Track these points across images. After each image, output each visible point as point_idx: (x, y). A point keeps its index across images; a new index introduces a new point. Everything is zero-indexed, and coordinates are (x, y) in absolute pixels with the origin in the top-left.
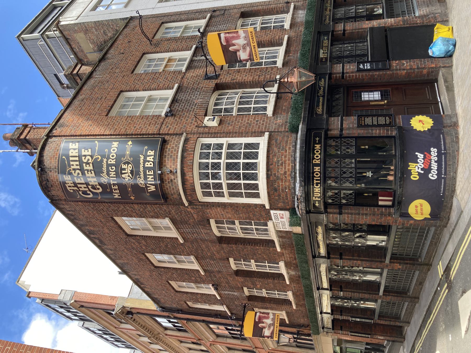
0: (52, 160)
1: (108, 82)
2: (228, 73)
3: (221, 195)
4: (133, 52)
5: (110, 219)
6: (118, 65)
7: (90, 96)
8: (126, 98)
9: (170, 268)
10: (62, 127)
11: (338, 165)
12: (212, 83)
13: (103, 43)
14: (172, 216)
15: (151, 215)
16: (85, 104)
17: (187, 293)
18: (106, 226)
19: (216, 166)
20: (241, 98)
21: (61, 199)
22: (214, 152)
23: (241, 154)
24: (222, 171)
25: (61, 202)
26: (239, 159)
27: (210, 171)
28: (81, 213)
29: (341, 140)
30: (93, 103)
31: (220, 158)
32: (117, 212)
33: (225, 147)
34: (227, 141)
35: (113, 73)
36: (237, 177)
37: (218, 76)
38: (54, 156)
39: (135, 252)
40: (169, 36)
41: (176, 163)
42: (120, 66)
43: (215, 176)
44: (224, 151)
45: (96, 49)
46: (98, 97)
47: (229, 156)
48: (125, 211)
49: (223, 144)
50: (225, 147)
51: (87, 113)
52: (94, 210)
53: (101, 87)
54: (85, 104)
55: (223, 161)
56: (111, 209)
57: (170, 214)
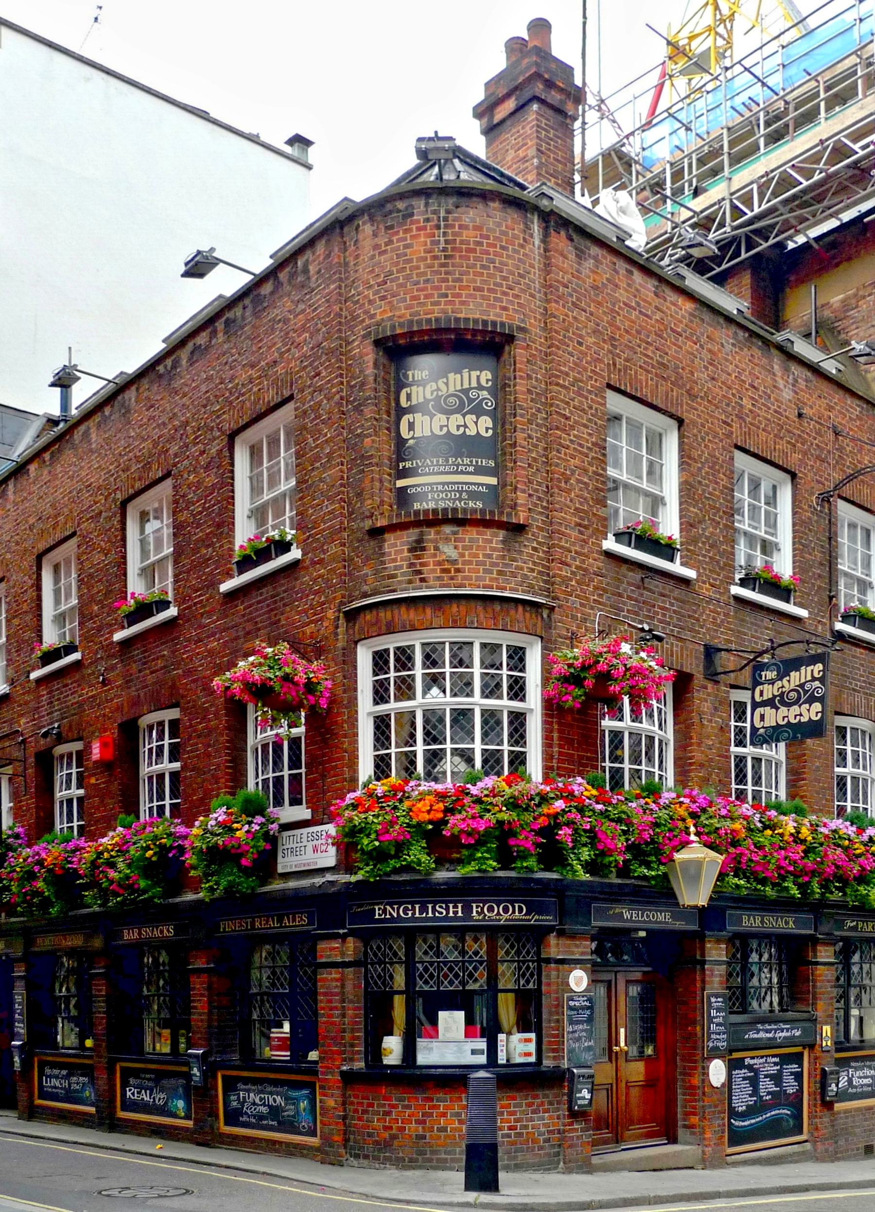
0: (472, 233)
1: (713, 379)
2: (721, 703)
3: (380, 695)
4: (803, 444)
5: (287, 393)
6: (763, 404)
7: (672, 329)
8: (660, 435)
9: (124, 546)
10: (577, 255)
11: (470, 957)
12: (694, 666)
13: (843, 336)
14: (307, 568)
15: (307, 510)
16: (647, 316)
17: (39, 588)
18: (260, 377)
19: (464, 686)
20: (651, 739)
21: (345, 250)
22: (501, 679)
23: (498, 745)
24: (449, 699)
25: (336, 249)
26: (483, 740)
27: (448, 670)
28: (301, 306)
29: (533, 962)
30: (648, 343)
31: (485, 695)
32: (313, 416)
33: (516, 705)
34: (531, 710)
35: (738, 392)
36: (431, 737)
37: (715, 678)
38: (488, 238)
39: (174, 449)
40: (844, 539)
41: (470, 585)
42: (760, 409)
43: (404, 658)
44: (504, 703)
45: (827, 313)
46: (667, 354)
47: (491, 718)
48: (317, 439)
49: (523, 699)
50: (516, 705)
51: (619, 329)
52: (313, 348)
53: (697, 361)
54: (647, 316)
55: (477, 701)
56: (322, 401)
57: (314, 563)
